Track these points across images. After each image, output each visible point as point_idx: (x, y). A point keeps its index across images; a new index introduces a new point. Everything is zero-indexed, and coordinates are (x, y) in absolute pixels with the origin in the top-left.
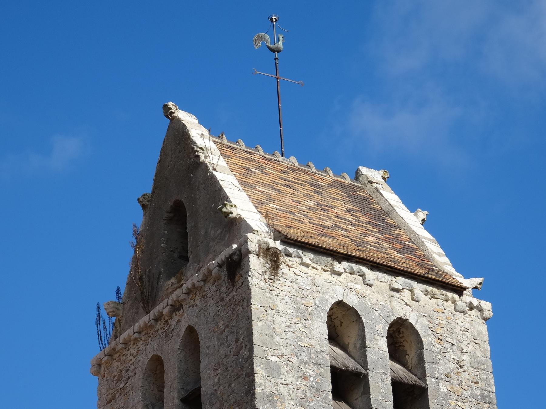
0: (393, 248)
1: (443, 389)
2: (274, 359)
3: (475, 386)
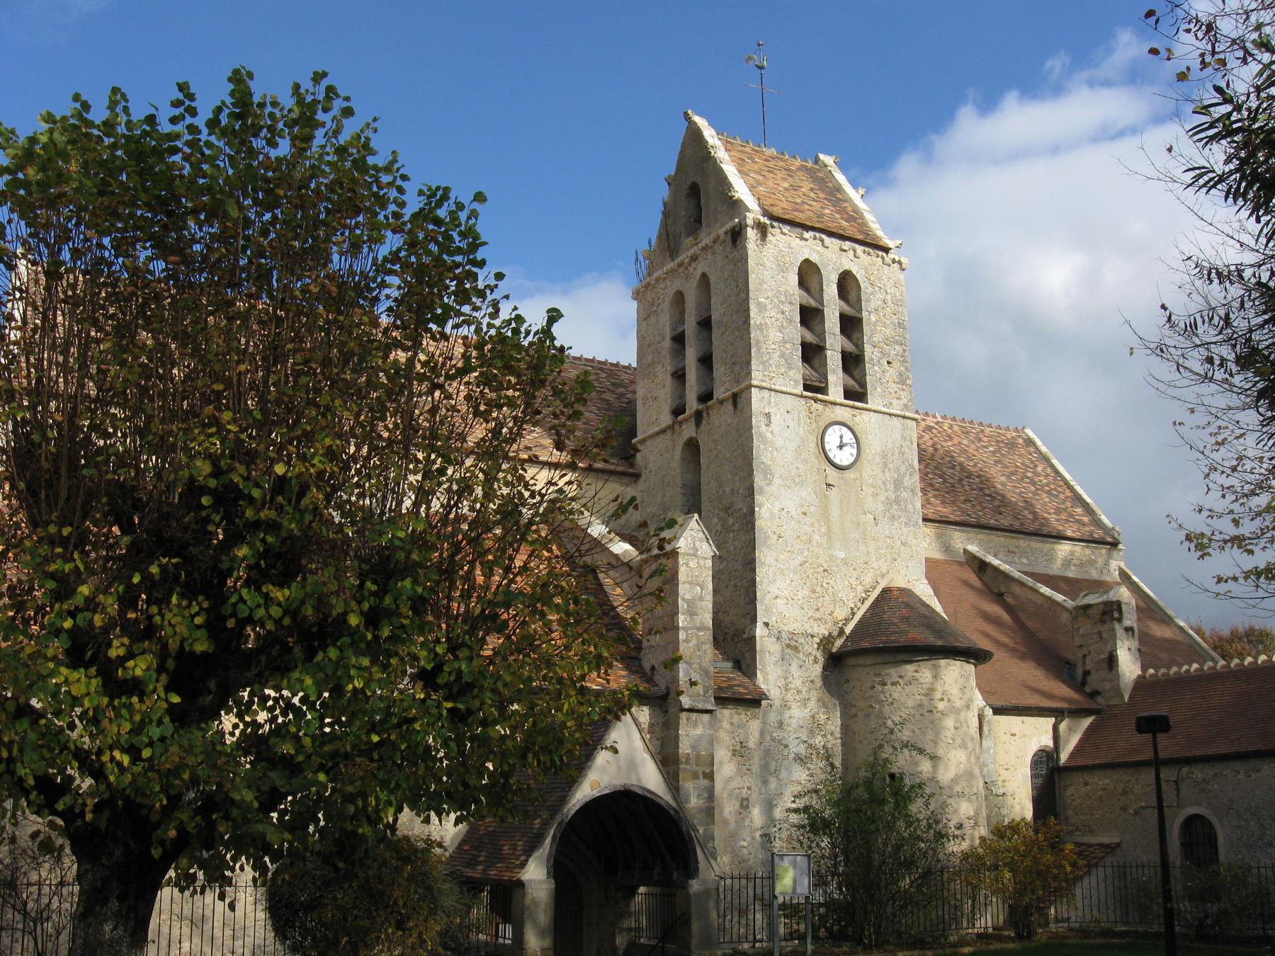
0: (842, 218)
1: (873, 319)
2: (763, 300)
3: (894, 317)
